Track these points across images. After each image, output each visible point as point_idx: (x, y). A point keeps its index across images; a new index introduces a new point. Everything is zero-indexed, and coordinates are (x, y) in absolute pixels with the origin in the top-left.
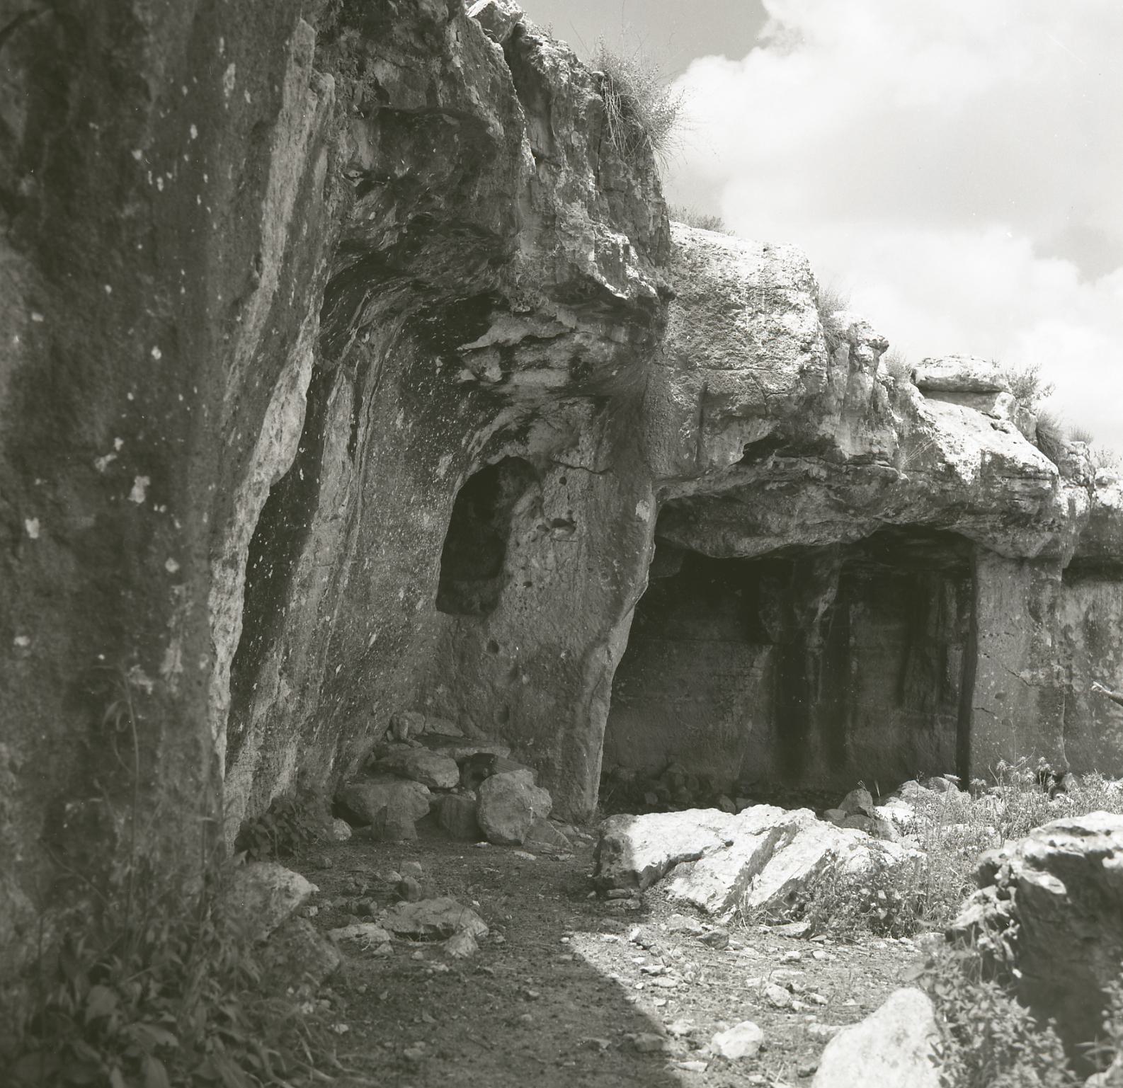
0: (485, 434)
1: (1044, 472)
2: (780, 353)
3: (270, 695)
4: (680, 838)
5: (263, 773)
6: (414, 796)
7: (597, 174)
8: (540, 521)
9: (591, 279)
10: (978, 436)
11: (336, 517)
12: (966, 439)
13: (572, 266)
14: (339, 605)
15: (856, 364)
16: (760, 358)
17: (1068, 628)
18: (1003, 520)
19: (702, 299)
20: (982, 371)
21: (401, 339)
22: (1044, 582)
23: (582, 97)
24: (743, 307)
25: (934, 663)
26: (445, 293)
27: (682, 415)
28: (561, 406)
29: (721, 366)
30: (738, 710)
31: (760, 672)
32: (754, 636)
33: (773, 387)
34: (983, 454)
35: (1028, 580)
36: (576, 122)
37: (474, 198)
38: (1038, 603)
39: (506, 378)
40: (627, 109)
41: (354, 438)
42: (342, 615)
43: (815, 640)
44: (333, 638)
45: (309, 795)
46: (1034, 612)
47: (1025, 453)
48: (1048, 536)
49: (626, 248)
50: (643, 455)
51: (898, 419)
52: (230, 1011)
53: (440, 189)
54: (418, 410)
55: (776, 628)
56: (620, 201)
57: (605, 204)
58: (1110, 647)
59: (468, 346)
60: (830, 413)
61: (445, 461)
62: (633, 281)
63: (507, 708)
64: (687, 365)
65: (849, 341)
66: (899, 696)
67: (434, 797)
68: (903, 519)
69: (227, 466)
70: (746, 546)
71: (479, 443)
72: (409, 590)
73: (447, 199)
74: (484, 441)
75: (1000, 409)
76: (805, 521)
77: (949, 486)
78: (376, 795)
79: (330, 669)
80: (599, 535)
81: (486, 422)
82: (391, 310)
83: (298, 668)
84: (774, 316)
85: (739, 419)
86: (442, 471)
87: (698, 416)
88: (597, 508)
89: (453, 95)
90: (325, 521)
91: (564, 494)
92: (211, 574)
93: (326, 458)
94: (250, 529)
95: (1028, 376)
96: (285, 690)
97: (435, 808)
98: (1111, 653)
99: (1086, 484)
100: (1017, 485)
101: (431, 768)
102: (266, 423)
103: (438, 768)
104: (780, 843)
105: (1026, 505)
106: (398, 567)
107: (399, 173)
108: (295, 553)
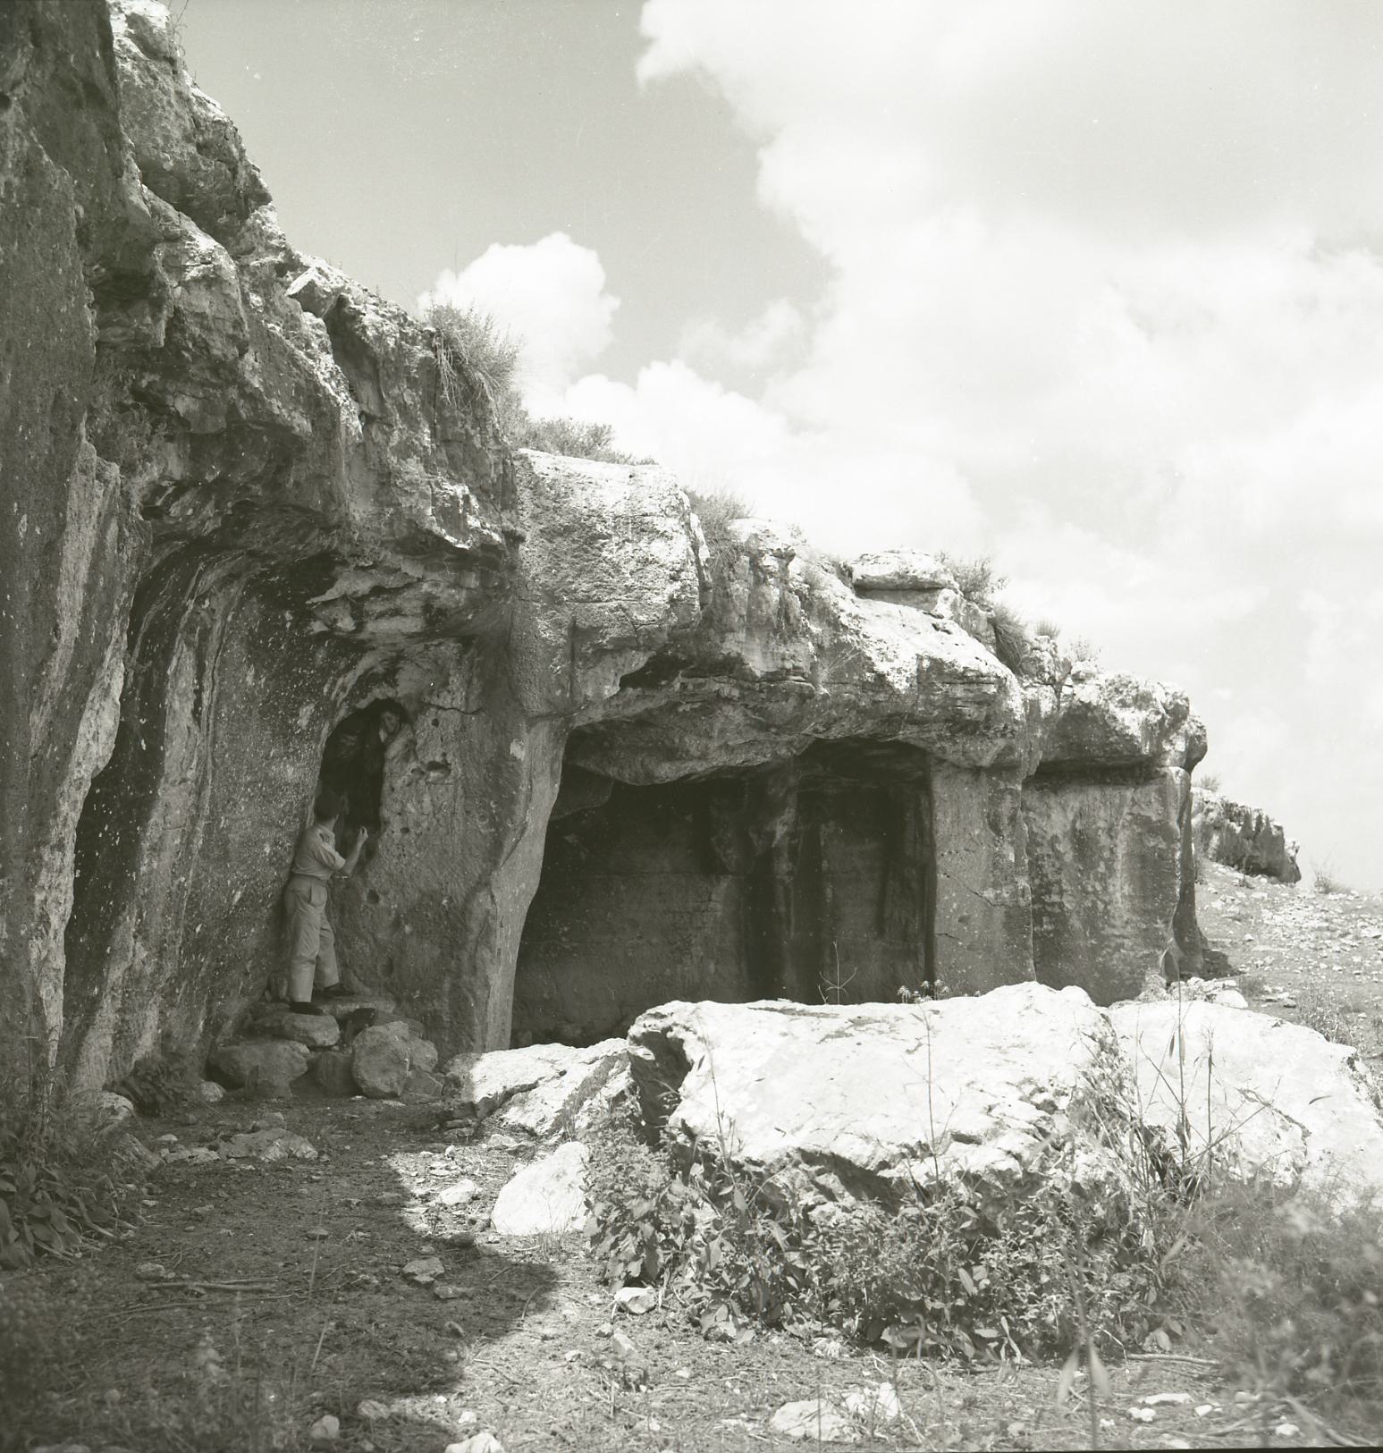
0: (350, 679)
1: (988, 675)
2: (654, 578)
3: (124, 958)
4: (518, 1071)
5: (124, 1037)
6: (289, 1057)
7: (433, 428)
8: (414, 765)
9: (430, 532)
10: (916, 639)
11: (184, 780)
12: (899, 643)
13: (410, 521)
14: (194, 865)
15: (759, 575)
16: (628, 589)
17: (1055, 838)
18: (949, 729)
19: (567, 531)
20: (923, 567)
21: (242, 602)
22: (1002, 792)
23: (413, 355)
24: (609, 537)
25: (914, 885)
26: (280, 558)
27: (551, 650)
28: (427, 647)
29: (588, 599)
30: (698, 951)
31: (719, 907)
32: (710, 867)
33: (643, 618)
34: (920, 658)
35: (986, 790)
36: (408, 380)
37: (290, 485)
38: (997, 816)
39: (360, 626)
40: (456, 361)
41: (198, 702)
42: (198, 875)
43: (783, 866)
44: (190, 898)
45: (176, 1056)
46: (994, 826)
47: (972, 655)
48: (1001, 743)
49: (466, 498)
50: (514, 693)
51: (815, 629)
52: (54, 1173)
53: (257, 480)
54: (270, 665)
55: (732, 856)
56: (458, 452)
57: (443, 456)
58: (1101, 858)
59: (315, 600)
60: (732, 631)
61: (306, 711)
62: (475, 531)
63: (391, 961)
64: (553, 599)
65: (749, 554)
66: (880, 925)
67: (312, 1056)
68: (835, 733)
69: (47, 773)
70: (666, 771)
71: (343, 688)
72: (276, 844)
73: (264, 487)
74: (349, 686)
75: (942, 607)
76: (721, 744)
77: (881, 697)
78: (249, 1056)
79: (189, 930)
80: (475, 776)
81: (348, 668)
82: (230, 575)
83: (155, 930)
84: (642, 544)
85: (611, 651)
86: (303, 722)
87: (568, 650)
88: (471, 749)
89: (255, 409)
90: (173, 784)
91: (436, 736)
92: (41, 858)
93: (170, 725)
94: (75, 816)
95: (978, 568)
96: (141, 953)
97: (313, 1066)
98: (1102, 864)
99: (1052, 682)
100: (959, 691)
101: (308, 1026)
102: (82, 729)
103: (317, 1025)
104: (614, 1070)
105: (970, 711)
106: (261, 822)
107: (209, 478)
108: (143, 819)
